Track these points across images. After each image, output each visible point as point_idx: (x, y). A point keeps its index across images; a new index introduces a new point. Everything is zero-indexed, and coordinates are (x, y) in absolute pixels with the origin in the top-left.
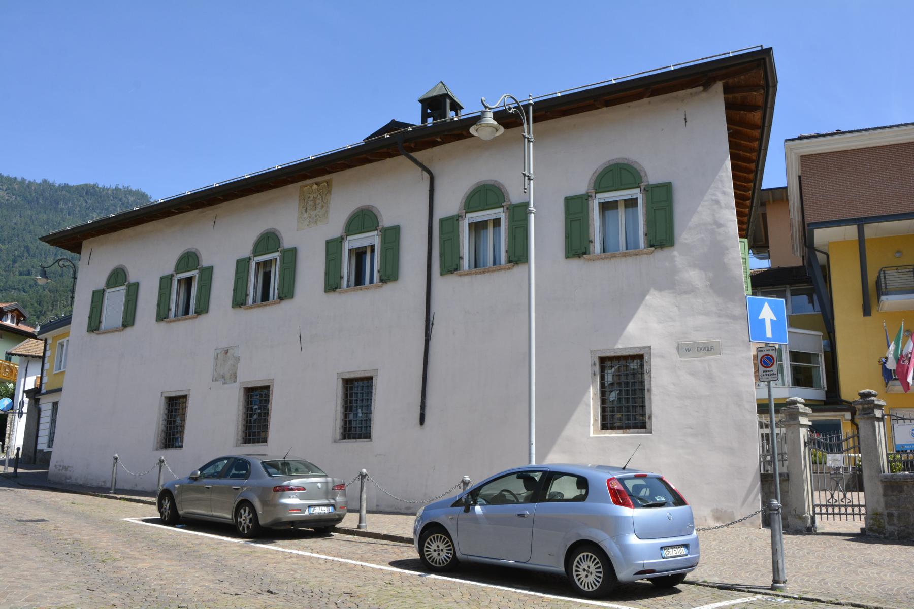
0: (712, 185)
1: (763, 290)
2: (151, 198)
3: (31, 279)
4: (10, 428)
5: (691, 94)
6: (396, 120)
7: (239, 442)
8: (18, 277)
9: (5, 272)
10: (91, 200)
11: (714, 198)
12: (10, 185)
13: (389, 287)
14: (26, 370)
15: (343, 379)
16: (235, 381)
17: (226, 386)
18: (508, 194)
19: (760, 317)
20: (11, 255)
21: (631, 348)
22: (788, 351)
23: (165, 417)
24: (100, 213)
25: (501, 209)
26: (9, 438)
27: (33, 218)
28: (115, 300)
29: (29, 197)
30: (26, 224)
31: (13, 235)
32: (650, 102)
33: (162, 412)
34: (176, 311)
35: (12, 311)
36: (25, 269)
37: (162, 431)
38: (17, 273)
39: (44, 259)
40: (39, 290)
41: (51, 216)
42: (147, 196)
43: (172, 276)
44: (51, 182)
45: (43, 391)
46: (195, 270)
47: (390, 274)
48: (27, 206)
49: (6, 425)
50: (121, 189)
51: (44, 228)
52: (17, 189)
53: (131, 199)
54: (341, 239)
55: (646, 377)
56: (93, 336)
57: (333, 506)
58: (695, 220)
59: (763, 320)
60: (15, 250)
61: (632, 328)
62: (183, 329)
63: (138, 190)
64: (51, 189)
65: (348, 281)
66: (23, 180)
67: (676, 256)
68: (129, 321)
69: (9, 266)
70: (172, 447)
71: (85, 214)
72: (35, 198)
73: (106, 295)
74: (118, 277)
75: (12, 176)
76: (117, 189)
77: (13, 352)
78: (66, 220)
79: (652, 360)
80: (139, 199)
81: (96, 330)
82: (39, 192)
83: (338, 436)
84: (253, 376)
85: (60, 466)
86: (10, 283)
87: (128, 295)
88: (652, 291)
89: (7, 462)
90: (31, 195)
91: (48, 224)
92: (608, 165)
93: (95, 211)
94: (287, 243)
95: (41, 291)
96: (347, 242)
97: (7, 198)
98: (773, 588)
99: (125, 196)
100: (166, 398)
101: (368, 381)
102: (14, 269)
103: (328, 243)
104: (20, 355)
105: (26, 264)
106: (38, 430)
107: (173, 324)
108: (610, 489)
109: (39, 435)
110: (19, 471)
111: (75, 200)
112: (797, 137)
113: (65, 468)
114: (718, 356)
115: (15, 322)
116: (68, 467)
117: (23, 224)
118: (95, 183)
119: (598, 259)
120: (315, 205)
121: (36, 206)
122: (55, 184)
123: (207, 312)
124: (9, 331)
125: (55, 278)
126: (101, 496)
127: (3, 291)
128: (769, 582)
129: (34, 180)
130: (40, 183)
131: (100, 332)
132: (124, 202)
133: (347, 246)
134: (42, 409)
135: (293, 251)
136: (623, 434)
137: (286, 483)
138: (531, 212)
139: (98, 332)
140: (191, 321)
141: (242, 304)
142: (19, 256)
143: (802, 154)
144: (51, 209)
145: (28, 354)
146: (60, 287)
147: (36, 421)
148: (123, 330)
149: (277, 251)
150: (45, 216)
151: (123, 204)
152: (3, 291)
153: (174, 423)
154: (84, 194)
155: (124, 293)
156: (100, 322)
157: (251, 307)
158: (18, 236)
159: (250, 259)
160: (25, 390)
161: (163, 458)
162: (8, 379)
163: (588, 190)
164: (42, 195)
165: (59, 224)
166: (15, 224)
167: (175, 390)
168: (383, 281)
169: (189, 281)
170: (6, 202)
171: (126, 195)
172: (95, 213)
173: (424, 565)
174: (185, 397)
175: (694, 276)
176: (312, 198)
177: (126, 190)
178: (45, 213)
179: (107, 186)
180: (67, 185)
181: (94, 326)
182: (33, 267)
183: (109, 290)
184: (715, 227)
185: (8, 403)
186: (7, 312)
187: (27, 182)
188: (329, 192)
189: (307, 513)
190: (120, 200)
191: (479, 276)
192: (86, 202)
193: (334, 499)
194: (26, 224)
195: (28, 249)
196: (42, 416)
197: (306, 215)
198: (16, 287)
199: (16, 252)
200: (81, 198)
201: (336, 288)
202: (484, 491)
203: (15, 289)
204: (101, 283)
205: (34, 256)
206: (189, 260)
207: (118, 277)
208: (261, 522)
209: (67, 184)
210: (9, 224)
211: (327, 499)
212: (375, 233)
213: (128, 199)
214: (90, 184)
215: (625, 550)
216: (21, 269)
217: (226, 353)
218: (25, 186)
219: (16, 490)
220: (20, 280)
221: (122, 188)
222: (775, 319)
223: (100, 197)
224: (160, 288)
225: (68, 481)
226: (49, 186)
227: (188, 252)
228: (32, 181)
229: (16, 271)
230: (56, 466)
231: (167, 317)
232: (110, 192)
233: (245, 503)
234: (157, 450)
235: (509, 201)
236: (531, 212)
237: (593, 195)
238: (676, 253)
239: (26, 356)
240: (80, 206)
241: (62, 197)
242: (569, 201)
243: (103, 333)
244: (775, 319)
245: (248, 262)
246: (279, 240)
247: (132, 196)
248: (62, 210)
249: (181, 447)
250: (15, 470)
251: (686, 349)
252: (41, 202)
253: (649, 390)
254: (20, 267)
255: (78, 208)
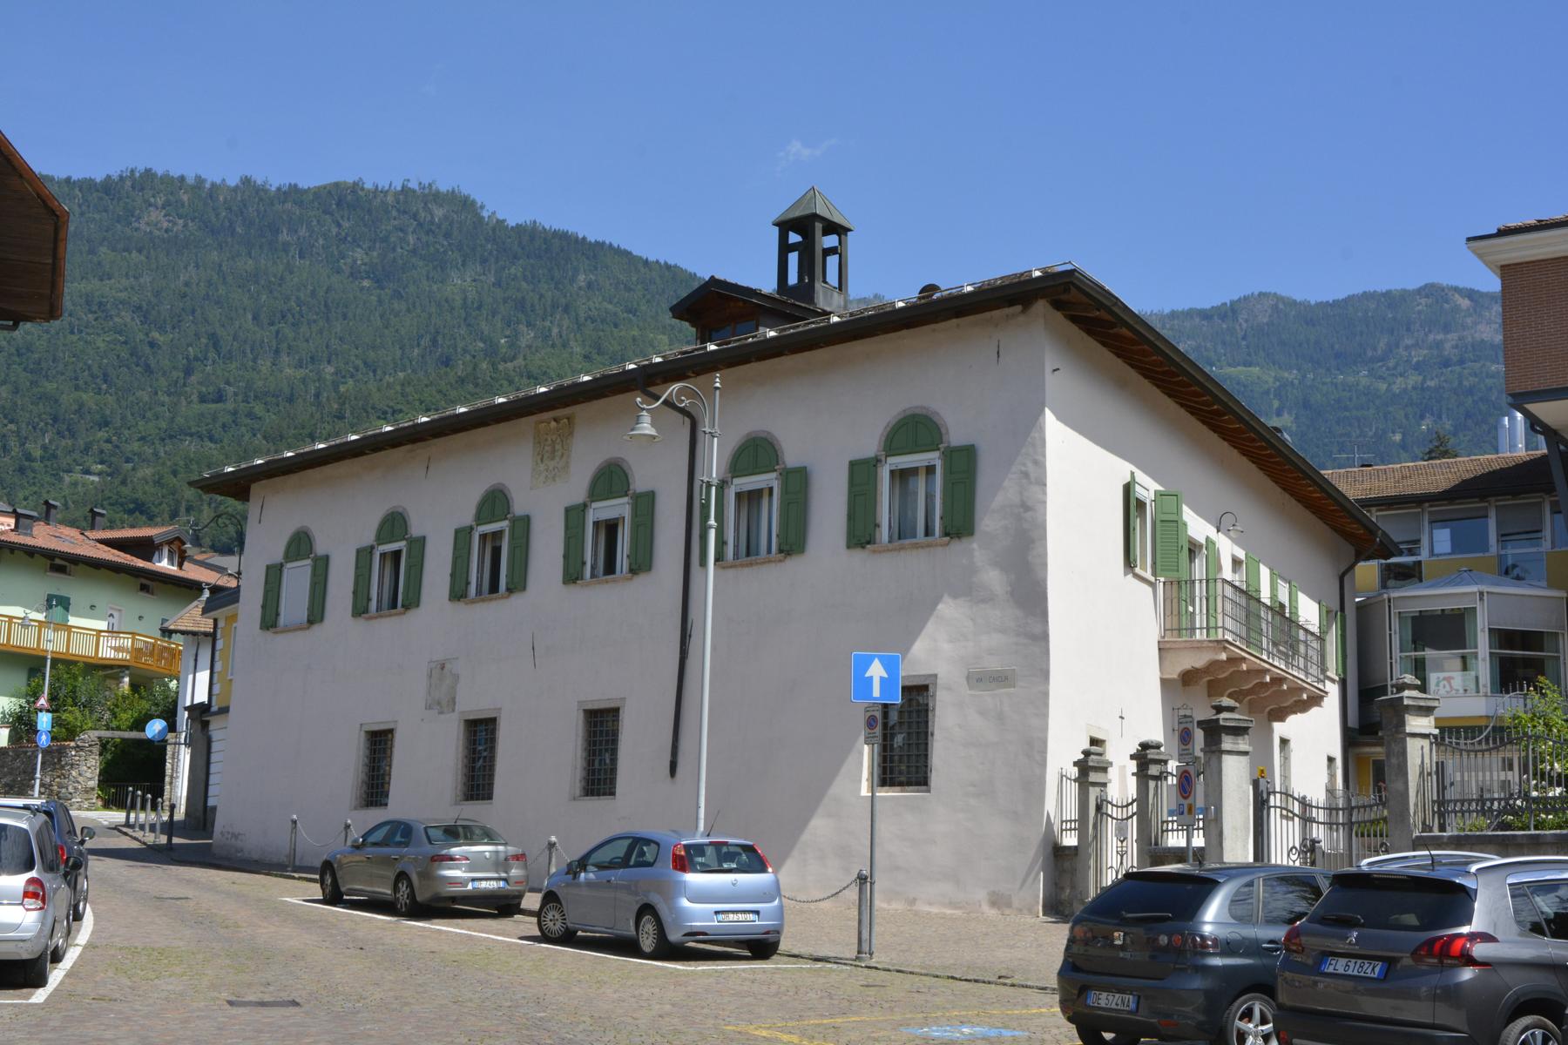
0: (1023, 451)
1: (1498, 503)
2: (482, 207)
3: (224, 410)
4: (173, 765)
5: (1007, 316)
6: (717, 277)
7: (459, 798)
8: (198, 407)
9: (168, 395)
10: (349, 219)
11: (1023, 469)
12: (172, 194)
13: (641, 579)
14: (196, 660)
15: (586, 711)
16: (453, 711)
17: (442, 716)
18: (783, 452)
19: (867, 675)
20: (180, 357)
21: (914, 676)
22: (1487, 630)
23: (366, 761)
24: (370, 248)
25: (774, 475)
26: (171, 783)
27: (224, 268)
28: (297, 578)
29: (214, 219)
30: (210, 283)
31: (183, 309)
32: (958, 325)
33: (361, 753)
34: (379, 601)
35: (170, 543)
36: (211, 389)
37: (363, 782)
38: (195, 398)
39: (251, 363)
40: (243, 436)
41: (263, 262)
42: (473, 203)
43: (372, 547)
44: (259, 182)
45: (214, 708)
46: (401, 540)
47: (642, 563)
48: (209, 241)
49: (165, 761)
50: (414, 191)
51: (249, 290)
52: (186, 204)
53: (439, 213)
54: (584, 507)
55: (930, 714)
56: (269, 635)
57: (505, 880)
58: (999, 500)
59: (871, 678)
60: (188, 345)
61: (919, 648)
62: (388, 628)
63: (453, 191)
64: (261, 199)
65: (593, 568)
66: (200, 181)
67: (975, 550)
68: (316, 615)
69: (177, 382)
70: (376, 805)
71: (336, 253)
72: (226, 221)
73: (285, 571)
74: (300, 545)
75: (175, 173)
76: (405, 190)
77: (172, 627)
78: (296, 270)
79: (938, 693)
80: (456, 213)
81: (272, 627)
82: (235, 208)
83: (578, 792)
84: (474, 703)
85: (228, 833)
86: (180, 420)
87: (314, 574)
88: (946, 598)
89: (158, 827)
90: (217, 215)
91: (257, 282)
92: (902, 416)
93: (359, 246)
94: (518, 508)
95: (246, 438)
96: (591, 511)
97: (165, 225)
98: (857, 958)
99: (426, 208)
100: (366, 732)
101: (614, 713)
102: (187, 389)
103: (568, 511)
104: (183, 633)
105: (213, 377)
106: (208, 774)
107: (374, 622)
108: (674, 854)
109: (211, 782)
110: (176, 840)
111: (315, 223)
112: (1495, 231)
113: (235, 836)
114: (1012, 690)
115: (176, 562)
116: (239, 834)
117: (202, 284)
118: (357, 179)
119: (884, 551)
120: (554, 451)
121: (229, 240)
122: (268, 187)
123: (418, 606)
124: (165, 582)
125: (278, 405)
126: (276, 876)
127: (167, 441)
128: (854, 954)
129: (224, 180)
130: (237, 186)
131: (278, 629)
132: (422, 220)
133: (591, 518)
134: (214, 739)
135: (526, 520)
136: (902, 792)
137: (444, 852)
138: (711, 527)
139: (274, 630)
140: (396, 617)
141: (462, 597)
142: (196, 359)
143: (1503, 263)
144: (261, 247)
145: (196, 629)
146: (289, 428)
147: (205, 758)
148: (308, 628)
149: (506, 519)
150: (250, 262)
151: (420, 225)
152: (167, 441)
153: (378, 771)
154: (334, 206)
155: (309, 570)
156: (277, 614)
157: (473, 602)
158: (193, 311)
159: (471, 528)
160: (195, 702)
161: (349, 821)
162: (167, 672)
163: (878, 451)
164: (242, 213)
165: (282, 278)
166: (187, 284)
167: (378, 722)
168: (634, 571)
169: (396, 555)
170: (166, 235)
171: (426, 204)
172: (359, 250)
173: (545, 937)
174: (391, 731)
175: (993, 579)
176: (549, 442)
177: (427, 191)
178: (249, 254)
179: (383, 184)
180: (294, 189)
181: (270, 620)
182: (228, 383)
183: (289, 565)
184: (1021, 510)
185: (160, 728)
186: (161, 544)
187: (208, 185)
188: (571, 434)
189: (470, 887)
190: (415, 217)
191: (746, 570)
192: (339, 226)
193: (506, 872)
194: (210, 283)
195: (215, 341)
196: (213, 750)
197: (542, 467)
198: (193, 430)
199: (190, 349)
200: (327, 216)
201: (577, 579)
202: (595, 858)
203: (191, 435)
204: (277, 555)
205: (230, 357)
206: (394, 524)
207: (300, 545)
208: (419, 899)
209: (296, 185)
210: (173, 286)
211: (497, 872)
212: (626, 499)
213: (431, 214)
214: (345, 182)
215: (679, 914)
216: (204, 389)
217: (443, 668)
218: (204, 195)
219: (165, 867)
220: (202, 415)
221: (417, 188)
222: (886, 676)
223: (369, 211)
224: (357, 568)
225: (239, 855)
226: (257, 193)
227: (393, 513)
228: (218, 182)
229: (193, 393)
230: (222, 833)
231: (366, 611)
232: (390, 199)
233: (402, 876)
234: (355, 808)
235: (784, 463)
236: (711, 527)
237: (883, 459)
238: (975, 546)
239: (194, 634)
240: (324, 235)
241: (285, 217)
242: (854, 466)
243: (282, 632)
244: (886, 676)
245: (470, 533)
246: (508, 502)
247: (441, 206)
248: (286, 247)
249: (386, 805)
250: (170, 839)
251: (981, 679)
252: (239, 230)
253: (932, 735)
254: (200, 383)
255: (321, 241)
